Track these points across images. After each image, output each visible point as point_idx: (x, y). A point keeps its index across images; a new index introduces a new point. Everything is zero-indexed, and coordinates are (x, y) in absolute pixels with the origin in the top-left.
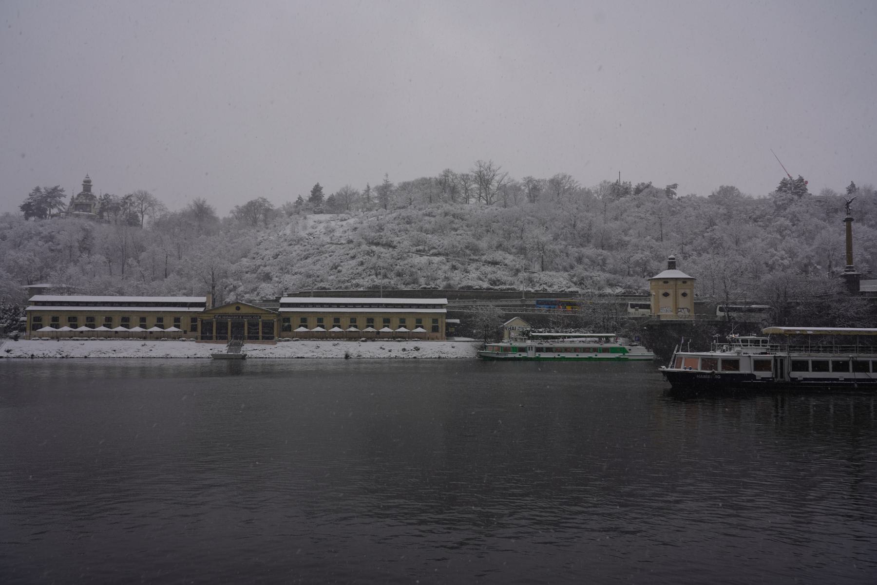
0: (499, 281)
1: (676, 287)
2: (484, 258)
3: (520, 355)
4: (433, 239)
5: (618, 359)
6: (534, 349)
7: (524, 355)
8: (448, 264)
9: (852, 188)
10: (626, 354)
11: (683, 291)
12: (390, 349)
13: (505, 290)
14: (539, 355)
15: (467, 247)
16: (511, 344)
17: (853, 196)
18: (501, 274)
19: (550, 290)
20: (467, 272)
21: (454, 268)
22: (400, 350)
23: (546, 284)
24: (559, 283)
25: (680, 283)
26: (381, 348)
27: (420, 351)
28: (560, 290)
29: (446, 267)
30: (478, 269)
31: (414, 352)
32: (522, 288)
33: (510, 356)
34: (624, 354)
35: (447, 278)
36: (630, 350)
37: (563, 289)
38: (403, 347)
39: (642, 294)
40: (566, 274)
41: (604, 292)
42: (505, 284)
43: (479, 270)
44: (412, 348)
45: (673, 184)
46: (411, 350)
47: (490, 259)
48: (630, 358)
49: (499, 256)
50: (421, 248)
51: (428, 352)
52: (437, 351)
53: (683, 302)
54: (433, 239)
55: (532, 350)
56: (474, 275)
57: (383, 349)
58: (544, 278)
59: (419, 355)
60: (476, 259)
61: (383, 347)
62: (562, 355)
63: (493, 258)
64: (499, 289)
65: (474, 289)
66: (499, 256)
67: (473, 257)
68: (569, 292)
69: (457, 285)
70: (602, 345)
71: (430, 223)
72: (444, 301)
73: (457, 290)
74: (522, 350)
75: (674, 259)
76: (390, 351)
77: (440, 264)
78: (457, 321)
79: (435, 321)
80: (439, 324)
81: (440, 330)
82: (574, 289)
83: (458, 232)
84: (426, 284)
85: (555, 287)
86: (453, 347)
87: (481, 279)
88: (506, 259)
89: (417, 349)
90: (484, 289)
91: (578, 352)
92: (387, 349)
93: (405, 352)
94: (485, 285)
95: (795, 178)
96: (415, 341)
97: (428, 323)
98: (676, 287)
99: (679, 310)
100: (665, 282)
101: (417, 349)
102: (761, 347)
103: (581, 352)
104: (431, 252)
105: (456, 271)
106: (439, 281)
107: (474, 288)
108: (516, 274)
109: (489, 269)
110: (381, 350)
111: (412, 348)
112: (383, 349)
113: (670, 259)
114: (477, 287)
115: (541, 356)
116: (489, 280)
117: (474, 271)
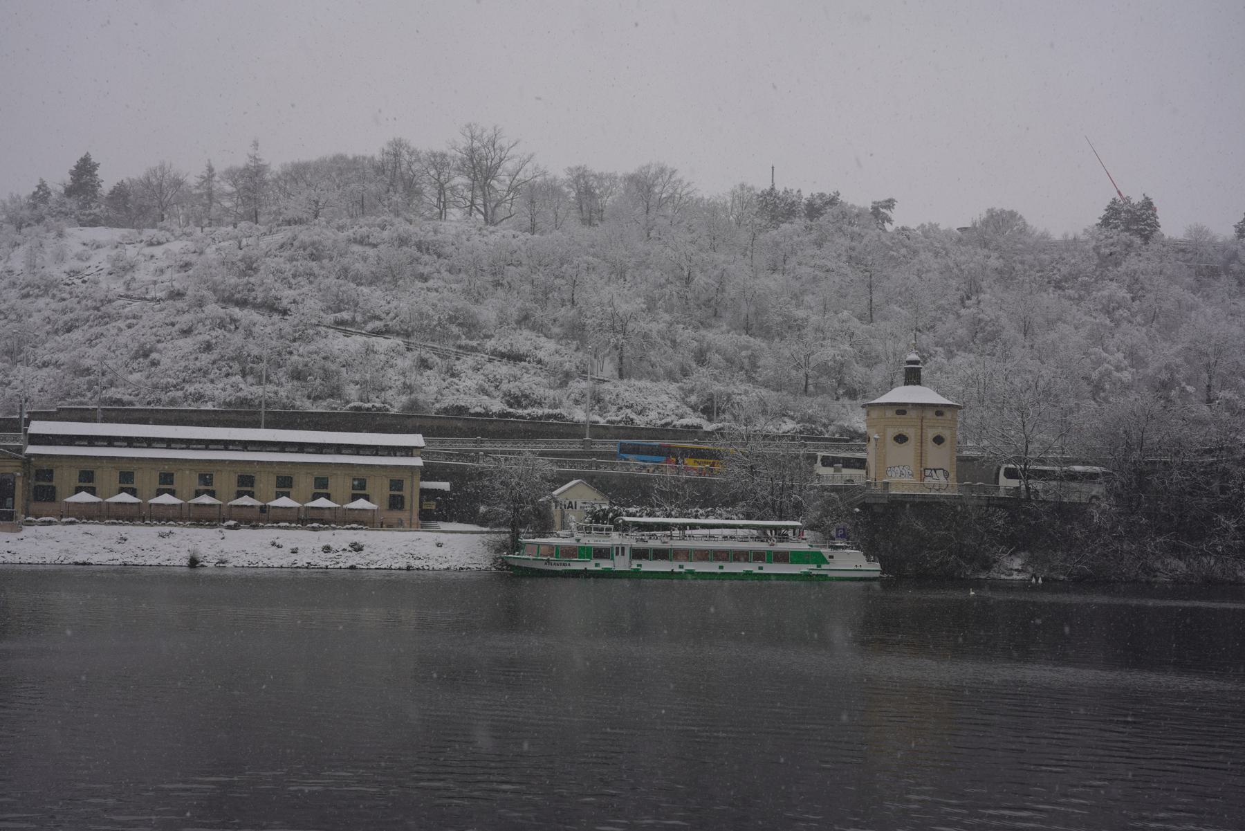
0: (527, 397)
2: (490, 344)
3: (597, 565)
4: (374, 297)
5: (807, 577)
6: (627, 552)
7: (605, 564)
8: (409, 354)
10: (824, 567)
12: (294, 547)
13: (540, 418)
15: (452, 319)
16: (578, 540)
18: (530, 381)
19: (640, 421)
20: (453, 375)
21: (424, 364)
22: (316, 550)
23: (631, 406)
24: (661, 405)
25: (930, 414)
26: (273, 544)
27: (363, 553)
28: (663, 422)
32: (579, 415)
34: (820, 566)
35: (408, 388)
36: (831, 557)
37: (668, 420)
38: (325, 544)
39: (837, 436)
40: (673, 387)
43: (481, 371)
44: (346, 546)
45: (886, 198)
46: (344, 550)
48: (831, 574)
49: (523, 340)
50: (346, 315)
52: (402, 553)
53: (939, 457)
54: (374, 297)
55: (623, 554)
56: (470, 381)
57: (278, 547)
58: (627, 394)
59: (362, 561)
60: (472, 347)
61: (278, 542)
62: (689, 566)
63: (512, 345)
64: (529, 414)
65: (471, 414)
66: (523, 340)
67: (464, 341)
68: (682, 426)
69: (433, 404)
71: (365, 259)
72: (416, 440)
73: (433, 415)
74: (601, 553)
75: (916, 362)
76: (294, 551)
77: (392, 354)
78: (445, 486)
79: (397, 485)
80: (406, 493)
82: (692, 419)
83: (430, 284)
85: (653, 415)
89: (357, 548)
91: (763, 561)
92: (288, 546)
94: (497, 406)
97: (378, 487)
99: (928, 472)
100: (939, 413)
101: (357, 548)
105: (429, 372)
106: (390, 392)
107: (472, 411)
108: (563, 384)
109: (503, 369)
110: (275, 548)
111: (346, 546)
112: (278, 547)
113: (909, 362)
114: (478, 410)
115: (643, 569)
117: (470, 372)
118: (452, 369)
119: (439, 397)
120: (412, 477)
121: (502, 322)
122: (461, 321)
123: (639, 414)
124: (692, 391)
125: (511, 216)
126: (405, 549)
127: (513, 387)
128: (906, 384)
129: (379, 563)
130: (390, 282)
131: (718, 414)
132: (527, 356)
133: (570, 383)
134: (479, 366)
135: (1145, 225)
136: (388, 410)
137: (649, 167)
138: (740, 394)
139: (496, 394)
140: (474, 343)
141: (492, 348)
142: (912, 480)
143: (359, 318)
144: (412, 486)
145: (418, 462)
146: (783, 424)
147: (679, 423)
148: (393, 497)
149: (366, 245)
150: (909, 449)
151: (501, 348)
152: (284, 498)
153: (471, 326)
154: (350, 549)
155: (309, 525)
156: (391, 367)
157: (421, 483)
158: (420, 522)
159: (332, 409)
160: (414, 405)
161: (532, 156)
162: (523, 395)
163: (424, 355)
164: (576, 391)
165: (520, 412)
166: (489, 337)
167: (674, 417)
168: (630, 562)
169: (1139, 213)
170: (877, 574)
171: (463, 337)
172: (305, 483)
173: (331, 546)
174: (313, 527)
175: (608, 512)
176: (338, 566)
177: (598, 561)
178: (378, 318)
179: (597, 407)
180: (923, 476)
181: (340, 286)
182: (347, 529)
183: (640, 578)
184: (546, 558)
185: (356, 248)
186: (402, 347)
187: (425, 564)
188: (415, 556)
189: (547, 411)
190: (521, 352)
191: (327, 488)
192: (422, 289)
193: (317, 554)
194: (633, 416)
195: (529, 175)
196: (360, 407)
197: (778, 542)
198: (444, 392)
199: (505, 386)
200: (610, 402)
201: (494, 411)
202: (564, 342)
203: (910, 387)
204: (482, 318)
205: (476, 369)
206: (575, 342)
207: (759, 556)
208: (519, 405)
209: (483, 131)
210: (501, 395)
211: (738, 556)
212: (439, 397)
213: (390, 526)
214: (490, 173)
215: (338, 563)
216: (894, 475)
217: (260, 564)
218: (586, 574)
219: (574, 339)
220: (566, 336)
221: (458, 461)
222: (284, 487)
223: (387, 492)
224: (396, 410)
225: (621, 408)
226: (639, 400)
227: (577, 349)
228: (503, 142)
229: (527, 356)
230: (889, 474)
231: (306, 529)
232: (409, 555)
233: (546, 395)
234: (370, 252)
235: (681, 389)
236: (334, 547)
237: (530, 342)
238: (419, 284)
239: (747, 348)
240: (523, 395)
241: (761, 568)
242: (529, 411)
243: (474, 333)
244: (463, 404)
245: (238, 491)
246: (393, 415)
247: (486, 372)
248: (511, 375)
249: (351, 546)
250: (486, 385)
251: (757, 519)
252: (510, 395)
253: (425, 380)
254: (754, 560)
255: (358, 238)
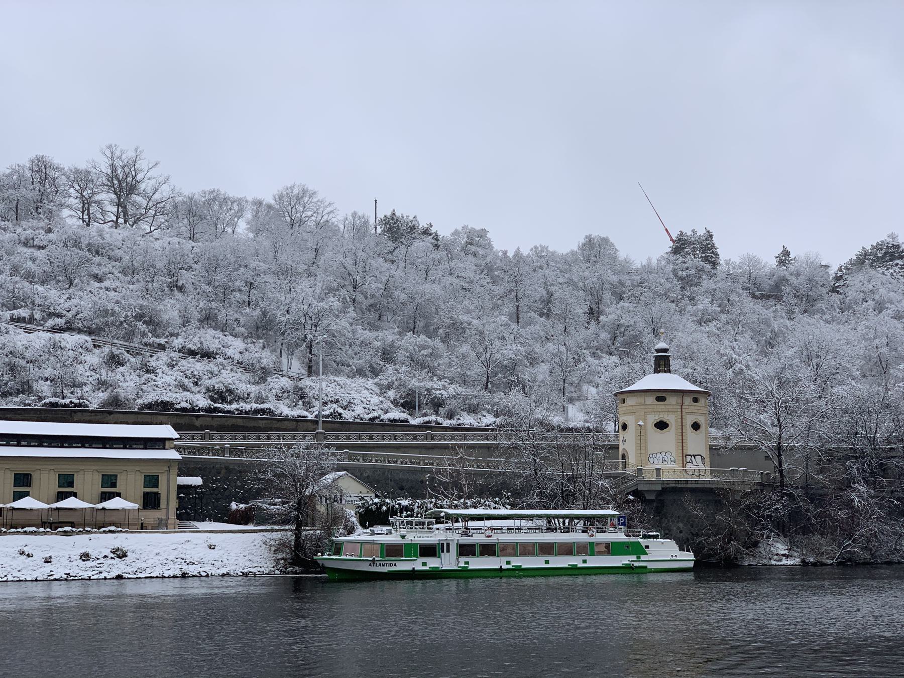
0: (231, 392)
1: (682, 408)
2: (177, 342)
3: (424, 564)
4: (53, 295)
5: (628, 569)
6: (453, 549)
7: (432, 563)
8: (97, 351)
9: (784, 257)
10: (643, 557)
11: (657, 418)
12: (47, 556)
13: (246, 413)
14: (467, 563)
15: (139, 317)
16: (403, 537)
17: (783, 271)
18: (230, 378)
19: (348, 416)
20: (148, 372)
21: (114, 361)
22: (73, 558)
23: (337, 401)
24: (364, 400)
25: (688, 400)
26: (22, 553)
27: (128, 560)
28: (371, 416)
29: (94, 359)
30: (173, 366)
31: (112, 561)
32: (285, 409)
33: (403, 566)
34: (639, 557)
35: (102, 384)
36: (647, 547)
37: (376, 414)
38: (83, 551)
40: (371, 383)
41: (459, 422)
42: (238, 399)
43: (177, 368)
44: (107, 552)
46: (105, 557)
47: (195, 345)
48: (650, 566)
49: (210, 338)
50: (23, 313)
51: (150, 562)
52: (172, 558)
53: (697, 443)
54: (53, 295)
55: (448, 551)
56: (168, 377)
57: (28, 556)
58: (329, 389)
59: (129, 569)
60: (159, 344)
61: (27, 550)
62: (516, 562)
63: (201, 343)
64: (237, 410)
65: (177, 410)
66: (210, 338)
67: (151, 339)
68: (390, 420)
69: (135, 400)
70: (592, 536)
71: (34, 260)
72: (165, 431)
73: (136, 410)
74: (429, 551)
75: (666, 350)
76: (48, 561)
77: (80, 350)
78: (197, 481)
79: (151, 481)
80: (162, 489)
81: (163, 504)
82: (397, 414)
83: (107, 283)
84: (55, 395)
85: (359, 410)
86: (211, 547)
87: (185, 389)
88: (228, 347)
89: (120, 554)
90: (201, 409)
91: (587, 554)
92: (39, 556)
93: (89, 564)
94: (202, 402)
95: (701, 232)
96: (111, 532)
97: (132, 483)
98: (682, 408)
99: (689, 458)
100: (661, 399)
101: (120, 554)
102: (426, 530)
103: (514, 555)
104: (50, 323)
105: (121, 369)
106: (85, 389)
107: (178, 407)
108: (263, 380)
109: (198, 366)
111: (107, 552)
112: (28, 556)
113: (658, 351)
114: (184, 405)
115: (470, 567)
116: (208, 390)
117: (165, 368)
118: (146, 365)
119: (141, 393)
120: (169, 471)
121: (186, 322)
122: (147, 319)
123: (345, 409)
124: (389, 386)
125: (151, 232)
126: (175, 554)
127: (214, 382)
128: (657, 371)
129: (148, 571)
130: (64, 281)
131: (420, 407)
132: (217, 354)
133: (269, 379)
134: (174, 363)
135: (711, 253)
136: (86, 406)
137: (292, 188)
138: (440, 389)
139: (196, 389)
140: (163, 341)
141: (180, 346)
142: (675, 466)
143: (38, 316)
144: (168, 481)
145: (173, 455)
146: (483, 418)
147: (385, 417)
148: (146, 495)
149: (30, 247)
150: (669, 437)
151: (190, 346)
152: (73, 498)
153: (154, 323)
154: (113, 556)
155: (60, 529)
156: (80, 363)
157: (178, 478)
158: (178, 522)
159: (25, 405)
160: (115, 401)
161: (167, 179)
162: (227, 391)
163: (116, 352)
164: (277, 387)
165: (227, 407)
166: (177, 335)
167: (380, 412)
168: (458, 559)
169: (705, 244)
170: (691, 565)
171: (150, 335)
172: (47, 481)
173: (90, 553)
174: (65, 532)
175: (381, 506)
176: (102, 576)
177: (424, 560)
178: (59, 316)
179: (300, 403)
180: (685, 463)
181: (16, 283)
182: (104, 532)
183: (467, 578)
184: (371, 559)
185: (21, 249)
186: (90, 345)
187: (201, 570)
188: (188, 561)
189: (255, 406)
190: (211, 350)
191: (73, 487)
192: (100, 288)
193: (75, 563)
194: (340, 410)
195: (166, 194)
196: (57, 404)
197: (597, 532)
198: (144, 387)
199: (207, 382)
200: (314, 397)
201: (201, 406)
202: (249, 340)
203: (662, 375)
204: (165, 317)
205: (171, 366)
206: (261, 341)
207: (546, 549)
208: (223, 400)
209: (122, 152)
210: (204, 391)
211: (526, 550)
212: (141, 393)
213: (143, 527)
214: (132, 189)
215: (101, 573)
216: (656, 462)
217: (10, 578)
218: (412, 575)
219: (259, 338)
220: (250, 335)
221: (201, 454)
222: (23, 486)
223: (141, 490)
224: (96, 406)
225: (326, 403)
226: (343, 396)
227: (264, 347)
228: (142, 164)
229: (217, 354)
230: (651, 460)
231: (56, 534)
232: (180, 560)
233: (249, 391)
234: (39, 254)
235: (378, 385)
236: (93, 554)
237: (218, 340)
238: (97, 284)
239: (424, 347)
240: (227, 391)
241: (585, 562)
242: (234, 406)
243: (159, 331)
244: (168, 399)
245: (102, 493)
246: (93, 411)
247: (183, 369)
248: (208, 371)
249: (114, 553)
250: (186, 381)
251: (521, 508)
252: (213, 391)
253: (119, 376)
254: (578, 553)
255: (23, 239)
